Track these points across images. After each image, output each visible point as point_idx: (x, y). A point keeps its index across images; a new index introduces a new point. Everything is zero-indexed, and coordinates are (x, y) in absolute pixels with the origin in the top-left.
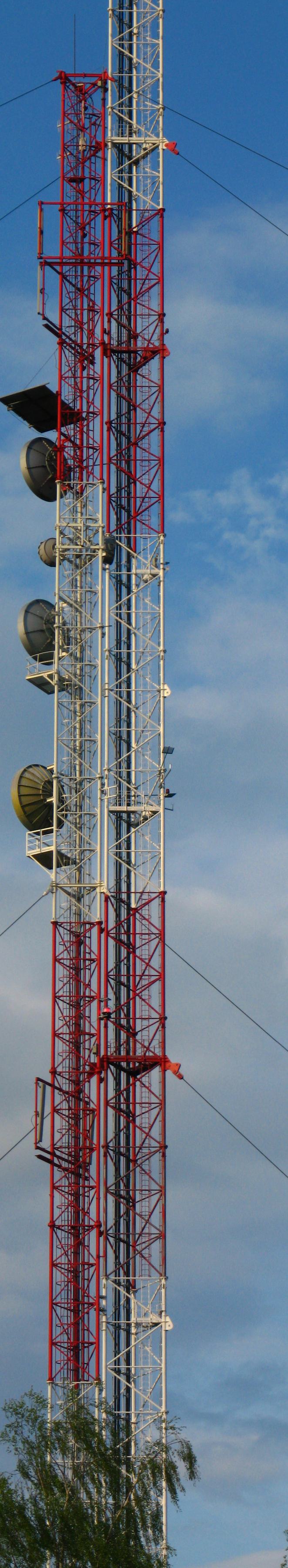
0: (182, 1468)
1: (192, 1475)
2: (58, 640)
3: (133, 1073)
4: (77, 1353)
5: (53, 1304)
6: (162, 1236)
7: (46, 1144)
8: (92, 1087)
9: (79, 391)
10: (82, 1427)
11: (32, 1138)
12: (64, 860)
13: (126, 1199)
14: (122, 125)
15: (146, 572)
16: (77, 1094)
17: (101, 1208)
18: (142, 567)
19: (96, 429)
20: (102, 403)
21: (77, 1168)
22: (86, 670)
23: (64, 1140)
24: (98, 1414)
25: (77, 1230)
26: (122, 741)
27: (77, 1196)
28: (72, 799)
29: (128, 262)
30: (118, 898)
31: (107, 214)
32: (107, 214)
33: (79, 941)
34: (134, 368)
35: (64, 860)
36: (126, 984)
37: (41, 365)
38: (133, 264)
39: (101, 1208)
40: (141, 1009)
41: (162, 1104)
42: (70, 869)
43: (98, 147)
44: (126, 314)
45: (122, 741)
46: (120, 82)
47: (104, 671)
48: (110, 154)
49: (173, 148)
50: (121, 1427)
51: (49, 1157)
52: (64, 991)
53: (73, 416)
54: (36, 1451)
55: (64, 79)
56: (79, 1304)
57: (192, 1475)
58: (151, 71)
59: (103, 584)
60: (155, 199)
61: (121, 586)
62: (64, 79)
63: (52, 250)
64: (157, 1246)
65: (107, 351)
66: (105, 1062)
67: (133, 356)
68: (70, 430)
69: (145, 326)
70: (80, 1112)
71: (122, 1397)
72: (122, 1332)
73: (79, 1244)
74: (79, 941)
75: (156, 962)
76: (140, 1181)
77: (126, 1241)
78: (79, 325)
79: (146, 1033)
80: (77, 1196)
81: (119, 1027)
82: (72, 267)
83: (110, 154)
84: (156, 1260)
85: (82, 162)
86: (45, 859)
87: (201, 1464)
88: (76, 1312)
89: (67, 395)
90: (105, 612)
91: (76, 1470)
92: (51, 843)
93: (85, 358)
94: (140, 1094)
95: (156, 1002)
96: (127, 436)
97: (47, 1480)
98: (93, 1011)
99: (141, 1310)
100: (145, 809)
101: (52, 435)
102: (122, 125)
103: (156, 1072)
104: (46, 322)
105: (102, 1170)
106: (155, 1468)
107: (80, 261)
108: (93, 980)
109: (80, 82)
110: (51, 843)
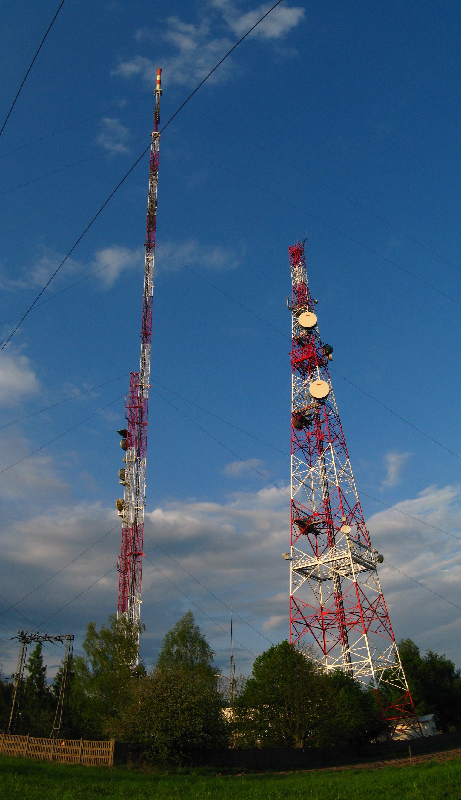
0: (143, 628)
1: (145, 630)
2: (126, 476)
3: (136, 556)
4: (123, 607)
5: (119, 597)
6: (140, 586)
7: (119, 568)
8: (129, 559)
9: (132, 431)
10: (124, 620)
11: (116, 568)
12: (125, 516)
13: (134, 579)
14: (141, 383)
15: (143, 464)
16: (125, 559)
17: (129, 580)
18: (142, 464)
19: (134, 438)
20: (136, 433)
21: (125, 573)
22: (131, 482)
23: (123, 568)
24: (127, 618)
25: (124, 584)
26: (137, 495)
27: (124, 578)
28: (127, 505)
29: (141, 407)
30: (135, 524)
31: (138, 399)
32: (138, 399)
33: (127, 531)
34: (142, 427)
35: (125, 516)
36: (135, 539)
37: (125, 426)
38: (142, 408)
39: (129, 580)
40: (138, 544)
41: (141, 578)
42: (126, 518)
43: (137, 386)
44: (141, 417)
45: (137, 495)
46: (142, 374)
47: (134, 481)
48: (139, 387)
49: (150, 387)
50: (131, 620)
51: (120, 571)
52: (124, 540)
53: (130, 435)
54: (114, 624)
55: (132, 373)
56: (124, 597)
57: (145, 630)
58: (147, 373)
59: (135, 467)
60: (142, 520)
61: (138, 467)
62: (132, 373)
63: (128, 405)
64: (139, 588)
65: (137, 424)
66: (131, 553)
67: (141, 425)
68: (129, 438)
69: (144, 419)
70: (126, 562)
71: (131, 615)
72: (132, 603)
73: (125, 587)
74: (127, 531)
75: (141, 536)
76: (137, 576)
77: (133, 587)
78: (132, 419)
79: (139, 548)
80: (124, 578)
81: (134, 547)
82: (131, 408)
83: (139, 387)
84: (139, 590)
85: (134, 389)
86: (122, 516)
87: (146, 628)
88: (123, 599)
89: (129, 431)
90: (135, 471)
91: (122, 628)
92: (123, 513)
93: (133, 425)
94: (138, 560)
95: (141, 543)
96: (140, 438)
97: (117, 629)
98: (129, 544)
99: (136, 600)
100: (141, 508)
101: (126, 439)
102: (141, 383)
103: (140, 556)
104: (294, 437)
105: (130, 573)
106: (137, 628)
107: (133, 407)
108: (130, 539)
109: (135, 374)
110: (123, 513)
